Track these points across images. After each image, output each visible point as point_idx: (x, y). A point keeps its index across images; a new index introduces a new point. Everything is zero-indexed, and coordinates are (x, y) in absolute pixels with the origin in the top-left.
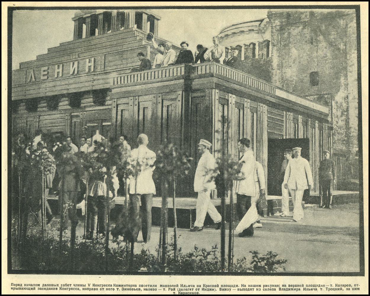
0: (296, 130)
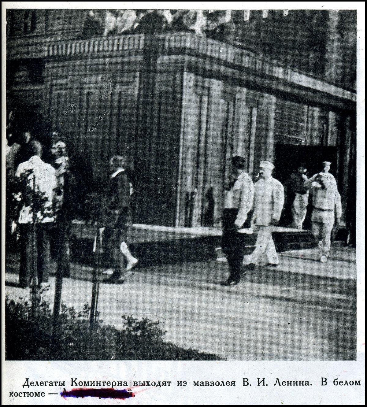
0: (324, 135)
